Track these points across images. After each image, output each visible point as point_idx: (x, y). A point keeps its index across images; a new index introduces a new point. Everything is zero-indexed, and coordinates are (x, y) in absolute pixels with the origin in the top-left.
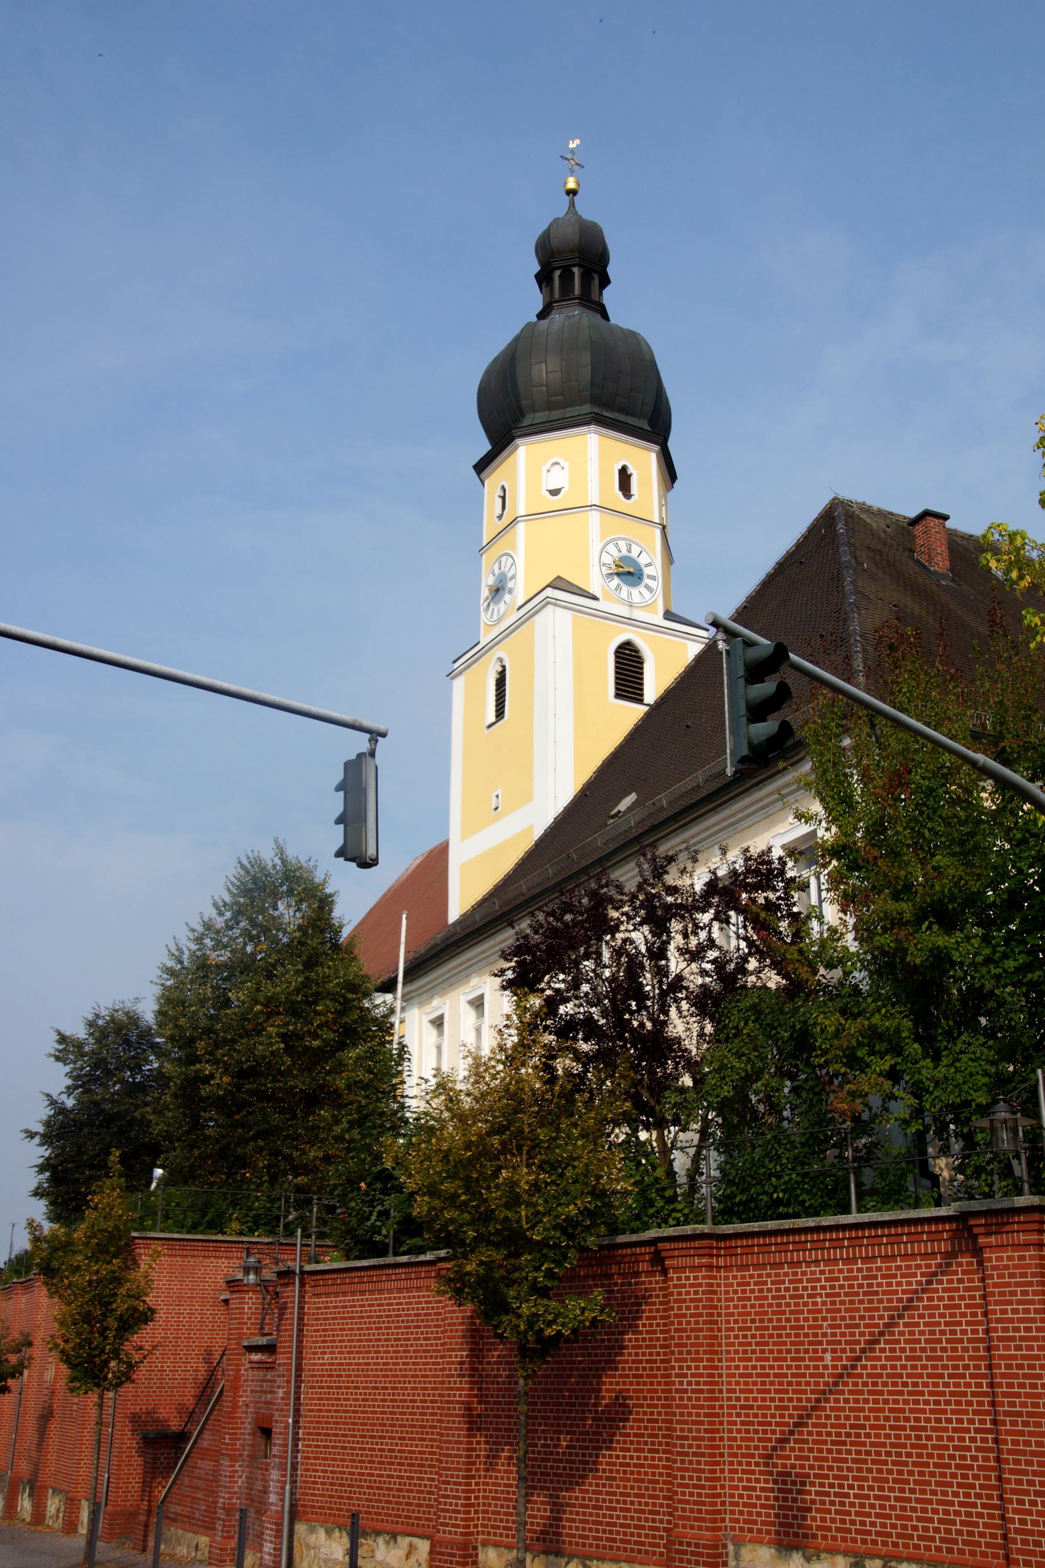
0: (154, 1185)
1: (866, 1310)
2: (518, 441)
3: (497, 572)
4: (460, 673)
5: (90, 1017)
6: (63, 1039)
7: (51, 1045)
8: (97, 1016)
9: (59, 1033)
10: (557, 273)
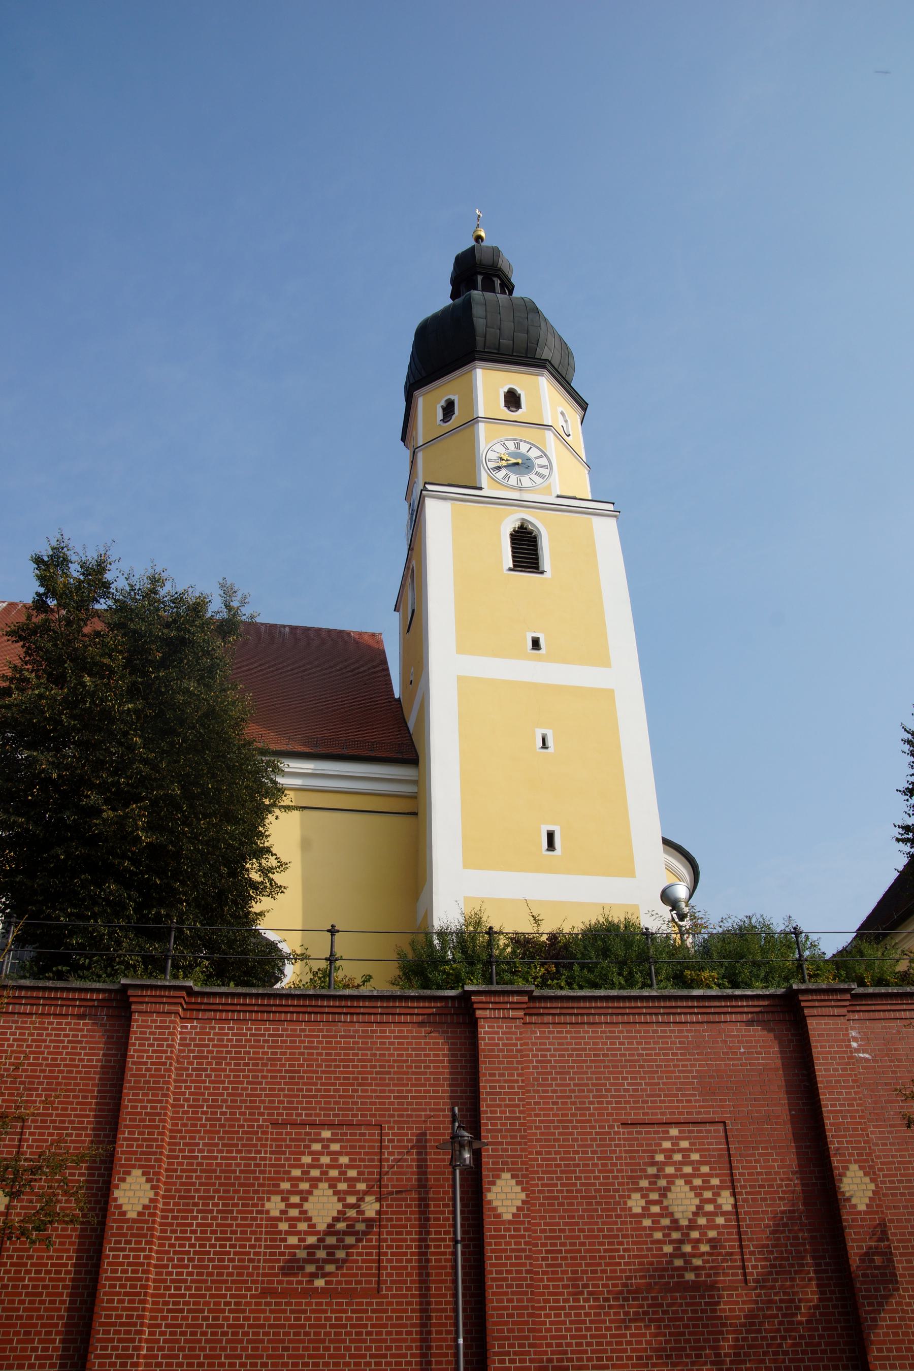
10: (480, 278)
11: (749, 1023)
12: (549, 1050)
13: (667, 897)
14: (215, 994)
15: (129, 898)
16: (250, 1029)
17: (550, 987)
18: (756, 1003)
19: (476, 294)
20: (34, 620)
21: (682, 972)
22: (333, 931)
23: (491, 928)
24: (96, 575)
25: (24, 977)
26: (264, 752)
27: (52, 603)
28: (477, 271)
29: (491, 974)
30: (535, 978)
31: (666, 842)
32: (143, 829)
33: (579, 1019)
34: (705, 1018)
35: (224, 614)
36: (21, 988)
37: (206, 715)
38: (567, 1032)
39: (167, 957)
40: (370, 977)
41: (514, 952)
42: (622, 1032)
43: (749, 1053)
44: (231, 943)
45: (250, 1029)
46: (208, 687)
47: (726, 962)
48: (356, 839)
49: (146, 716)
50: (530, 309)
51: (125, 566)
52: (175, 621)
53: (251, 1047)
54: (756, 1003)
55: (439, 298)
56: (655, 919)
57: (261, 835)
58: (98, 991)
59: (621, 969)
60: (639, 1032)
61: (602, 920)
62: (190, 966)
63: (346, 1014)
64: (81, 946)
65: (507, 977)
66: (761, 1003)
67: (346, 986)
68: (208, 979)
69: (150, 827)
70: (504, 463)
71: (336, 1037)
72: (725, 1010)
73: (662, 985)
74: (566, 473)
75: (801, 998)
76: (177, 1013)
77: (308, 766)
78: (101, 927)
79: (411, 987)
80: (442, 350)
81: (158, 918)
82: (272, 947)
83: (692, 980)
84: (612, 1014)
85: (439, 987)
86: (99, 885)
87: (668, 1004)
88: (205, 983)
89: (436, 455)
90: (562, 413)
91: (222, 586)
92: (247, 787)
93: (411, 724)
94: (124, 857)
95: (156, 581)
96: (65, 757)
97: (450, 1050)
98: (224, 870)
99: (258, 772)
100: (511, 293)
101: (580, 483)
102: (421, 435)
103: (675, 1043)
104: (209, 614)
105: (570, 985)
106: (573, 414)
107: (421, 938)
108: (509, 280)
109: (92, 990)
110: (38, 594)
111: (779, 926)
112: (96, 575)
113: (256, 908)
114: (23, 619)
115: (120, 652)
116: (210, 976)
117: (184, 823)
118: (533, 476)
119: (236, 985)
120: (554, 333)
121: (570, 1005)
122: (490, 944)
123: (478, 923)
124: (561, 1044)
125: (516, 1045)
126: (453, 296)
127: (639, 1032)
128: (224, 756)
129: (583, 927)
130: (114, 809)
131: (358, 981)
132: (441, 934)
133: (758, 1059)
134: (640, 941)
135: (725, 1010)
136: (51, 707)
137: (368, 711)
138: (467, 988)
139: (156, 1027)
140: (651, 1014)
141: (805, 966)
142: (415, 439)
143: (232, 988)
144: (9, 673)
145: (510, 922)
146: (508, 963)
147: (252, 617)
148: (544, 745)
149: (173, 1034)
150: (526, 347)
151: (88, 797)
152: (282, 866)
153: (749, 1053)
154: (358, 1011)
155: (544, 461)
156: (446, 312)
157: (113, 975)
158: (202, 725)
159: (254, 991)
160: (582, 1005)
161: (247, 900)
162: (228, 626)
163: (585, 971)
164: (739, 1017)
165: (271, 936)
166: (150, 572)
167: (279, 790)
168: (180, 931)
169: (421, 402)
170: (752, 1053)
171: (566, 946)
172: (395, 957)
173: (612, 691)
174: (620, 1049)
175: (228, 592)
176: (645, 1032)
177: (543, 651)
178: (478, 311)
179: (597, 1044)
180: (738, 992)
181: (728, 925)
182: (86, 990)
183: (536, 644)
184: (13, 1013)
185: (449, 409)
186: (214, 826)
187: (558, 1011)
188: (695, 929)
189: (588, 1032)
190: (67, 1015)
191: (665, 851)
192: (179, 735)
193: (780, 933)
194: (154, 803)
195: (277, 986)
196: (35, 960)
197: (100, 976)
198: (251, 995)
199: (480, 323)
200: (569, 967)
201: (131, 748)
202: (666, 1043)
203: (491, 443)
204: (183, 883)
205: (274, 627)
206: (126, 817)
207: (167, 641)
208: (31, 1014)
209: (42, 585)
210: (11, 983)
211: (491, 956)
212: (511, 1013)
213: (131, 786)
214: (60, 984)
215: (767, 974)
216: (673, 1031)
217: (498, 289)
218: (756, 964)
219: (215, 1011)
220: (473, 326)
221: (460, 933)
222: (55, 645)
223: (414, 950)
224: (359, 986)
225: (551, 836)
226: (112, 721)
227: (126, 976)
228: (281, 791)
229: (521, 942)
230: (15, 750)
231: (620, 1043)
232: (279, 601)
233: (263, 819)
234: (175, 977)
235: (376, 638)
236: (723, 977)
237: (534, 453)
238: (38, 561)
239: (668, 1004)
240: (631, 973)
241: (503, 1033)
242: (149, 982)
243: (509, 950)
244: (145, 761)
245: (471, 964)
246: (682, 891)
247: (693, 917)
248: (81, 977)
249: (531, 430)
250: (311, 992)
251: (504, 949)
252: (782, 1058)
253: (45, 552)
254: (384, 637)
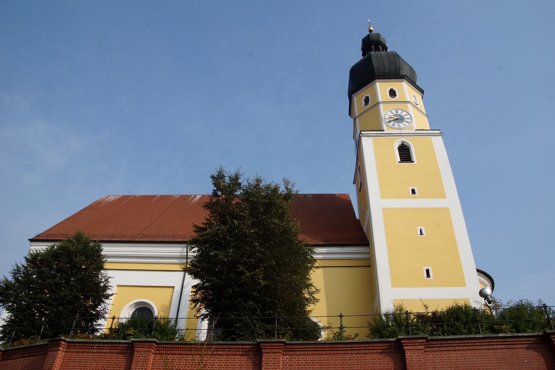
10: (373, 46)
11: (527, 348)
12: (437, 362)
13: (482, 294)
14: (295, 344)
15: (258, 307)
16: (310, 358)
17: (435, 335)
18: (529, 339)
19: (372, 53)
20: (213, 200)
21: (493, 326)
22: (341, 316)
23: (407, 311)
24: (235, 180)
25: (219, 340)
26: (306, 245)
27: (219, 193)
28: (372, 44)
29: (409, 331)
30: (428, 332)
31: (478, 271)
32: (262, 279)
33: (449, 349)
34: (506, 346)
35: (286, 192)
36: (219, 344)
37: (283, 232)
38: (444, 354)
39: (274, 330)
40: (358, 334)
41: (417, 321)
42: (468, 354)
43: (529, 362)
44: (299, 324)
45: (310, 358)
46: (282, 221)
47: (513, 321)
48: (348, 277)
49: (259, 234)
50: (395, 56)
51: (246, 176)
52: (267, 196)
53: (311, 365)
54: (529, 339)
55: (358, 56)
56: (478, 303)
57: (308, 279)
58: (249, 345)
59: (465, 326)
60: (476, 353)
61: (454, 305)
62: (283, 333)
63: (349, 350)
64: (240, 327)
65: (416, 331)
66: (532, 339)
67: (348, 339)
68: (291, 338)
69: (264, 278)
70: (392, 119)
71: (345, 360)
72: (515, 343)
73: (484, 332)
74: (418, 120)
75: (552, 337)
76: (280, 352)
77: (324, 250)
78: (247, 319)
79: (375, 338)
80: (362, 77)
81: (270, 315)
82: (315, 324)
83: (498, 330)
84: (463, 346)
85: (387, 337)
86: (246, 303)
87: (488, 341)
88: (290, 340)
89: (364, 119)
90: (414, 96)
91: (284, 181)
92: (301, 260)
93: (365, 230)
94: (255, 291)
95: (258, 181)
96: (229, 252)
97: (394, 364)
98: (295, 294)
99: (305, 253)
100: (386, 50)
101: (425, 124)
102: (357, 112)
103: (493, 358)
104: (280, 192)
105: (443, 334)
106: (418, 96)
107: (378, 317)
108: (385, 45)
109: (246, 345)
110: (214, 190)
111: (535, 304)
112: (235, 180)
113: (308, 308)
114: (209, 200)
115: (247, 210)
116: (292, 337)
117: (277, 276)
118: (405, 123)
119: (303, 340)
120: (406, 64)
121: (444, 342)
122: (407, 318)
123: (401, 309)
124: (442, 360)
125: (422, 361)
126: (363, 55)
127: (476, 353)
128: (291, 248)
129: (446, 309)
130: (250, 272)
131: (353, 336)
132: (386, 315)
133: (534, 365)
134: (472, 313)
135: (515, 343)
136: (222, 233)
137: (344, 224)
138: (399, 337)
139: (273, 359)
140: (481, 345)
141: (551, 322)
142: (355, 114)
143: (301, 342)
144: (206, 222)
145: (416, 309)
146: (415, 326)
147: (297, 192)
148: (421, 234)
149: (279, 361)
150: (396, 71)
151: (239, 268)
152: (317, 291)
153: (529, 362)
154: (354, 349)
155: (408, 116)
156: (361, 62)
157: (254, 338)
158: (281, 236)
159: (311, 342)
160: (449, 342)
161: (304, 305)
162: (288, 196)
163: (450, 327)
164: (522, 346)
165: (315, 320)
166: (256, 178)
167: (314, 260)
168: (279, 319)
169: (355, 99)
170: (531, 362)
171: (440, 317)
172: (367, 325)
173: (447, 209)
174: (468, 361)
175: (286, 183)
176: (479, 353)
177: (417, 194)
178: (374, 59)
179: (458, 359)
180: (520, 335)
181: (511, 304)
182: (244, 345)
183: (413, 192)
184: (216, 355)
185: (367, 100)
186: (289, 276)
187: (439, 345)
188: (496, 307)
189: (453, 354)
190: (237, 355)
191: (478, 275)
192: (272, 241)
193: (537, 307)
194: (265, 268)
195: (320, 340)
196: (223, 333)
197: (249, 339)
198: (309, 344)
199: (375, 64)
200: (442, 326)
201: (254, 247)
202: (489, 358)
203: (386, 112)
204: (279, 300)
205: (305, 195)
206: (254, 275)
207: (264, 204)
208: (223, 355)
209: (215, 187)
210: (214, 343)
211: (408, 323)
212: (419, 347)
213: (256, 262)
214: (234, 342)
215: (533, 326)
216: (492, 353)
217: (381, 50)
218: (527, 321)
219: (296, 351)
220: (374, 65)
221: (394, 314)
222: (222, 209)
223: (375, 322)
224: (353, 338)
225: (428, 271)
226: (246, 237)
227: (259, 338)
228: (315, 260)
229: (420, 316)
230: (210, 251)
231: (476, 358)
232: (307, 185)
233: (308, 273)
234: (278, 338)
235: (347, 196)
236: (512, 328)
237: (404, 114)
238: (213, 177)
239: (488, 341)
240: (470, 328)
241: (416, 356)
242: (268, 340)
243: (415, 320)
244: (260, 252)
245: (400, 327)
246: (488, 291)
247: (495, 302)
248: (241, 340)
249: (401, 104)
250: (334, 342)
251: (413, 320)
252: (546, 365)
253: (215, 174)
254: (350, 195)
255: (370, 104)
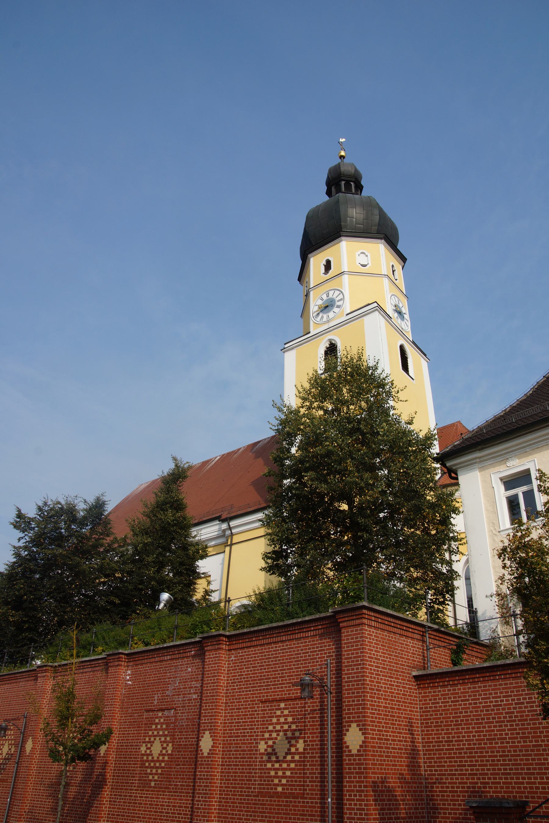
0: (162, 605)
1: (455, 733)
2: (343, 238)
3: (330, 296)
4: (293, 349)
5: (41, 504)
6: (20, 515)
7: (12, 516)
8: (45, 504)
9: (19, 511)
10: (343, 182)
95: (262, 569)
142: (308, 283)
185: (328, 266)
238: (12, 524)
255: (331, 273)
